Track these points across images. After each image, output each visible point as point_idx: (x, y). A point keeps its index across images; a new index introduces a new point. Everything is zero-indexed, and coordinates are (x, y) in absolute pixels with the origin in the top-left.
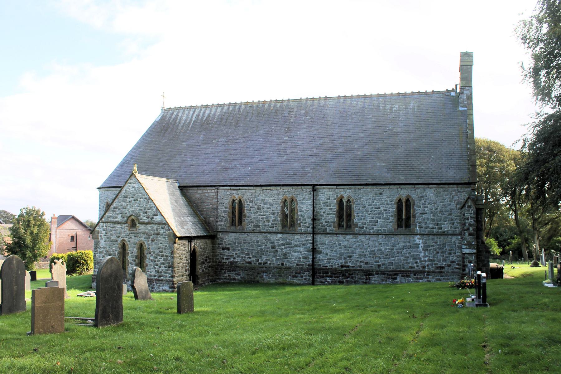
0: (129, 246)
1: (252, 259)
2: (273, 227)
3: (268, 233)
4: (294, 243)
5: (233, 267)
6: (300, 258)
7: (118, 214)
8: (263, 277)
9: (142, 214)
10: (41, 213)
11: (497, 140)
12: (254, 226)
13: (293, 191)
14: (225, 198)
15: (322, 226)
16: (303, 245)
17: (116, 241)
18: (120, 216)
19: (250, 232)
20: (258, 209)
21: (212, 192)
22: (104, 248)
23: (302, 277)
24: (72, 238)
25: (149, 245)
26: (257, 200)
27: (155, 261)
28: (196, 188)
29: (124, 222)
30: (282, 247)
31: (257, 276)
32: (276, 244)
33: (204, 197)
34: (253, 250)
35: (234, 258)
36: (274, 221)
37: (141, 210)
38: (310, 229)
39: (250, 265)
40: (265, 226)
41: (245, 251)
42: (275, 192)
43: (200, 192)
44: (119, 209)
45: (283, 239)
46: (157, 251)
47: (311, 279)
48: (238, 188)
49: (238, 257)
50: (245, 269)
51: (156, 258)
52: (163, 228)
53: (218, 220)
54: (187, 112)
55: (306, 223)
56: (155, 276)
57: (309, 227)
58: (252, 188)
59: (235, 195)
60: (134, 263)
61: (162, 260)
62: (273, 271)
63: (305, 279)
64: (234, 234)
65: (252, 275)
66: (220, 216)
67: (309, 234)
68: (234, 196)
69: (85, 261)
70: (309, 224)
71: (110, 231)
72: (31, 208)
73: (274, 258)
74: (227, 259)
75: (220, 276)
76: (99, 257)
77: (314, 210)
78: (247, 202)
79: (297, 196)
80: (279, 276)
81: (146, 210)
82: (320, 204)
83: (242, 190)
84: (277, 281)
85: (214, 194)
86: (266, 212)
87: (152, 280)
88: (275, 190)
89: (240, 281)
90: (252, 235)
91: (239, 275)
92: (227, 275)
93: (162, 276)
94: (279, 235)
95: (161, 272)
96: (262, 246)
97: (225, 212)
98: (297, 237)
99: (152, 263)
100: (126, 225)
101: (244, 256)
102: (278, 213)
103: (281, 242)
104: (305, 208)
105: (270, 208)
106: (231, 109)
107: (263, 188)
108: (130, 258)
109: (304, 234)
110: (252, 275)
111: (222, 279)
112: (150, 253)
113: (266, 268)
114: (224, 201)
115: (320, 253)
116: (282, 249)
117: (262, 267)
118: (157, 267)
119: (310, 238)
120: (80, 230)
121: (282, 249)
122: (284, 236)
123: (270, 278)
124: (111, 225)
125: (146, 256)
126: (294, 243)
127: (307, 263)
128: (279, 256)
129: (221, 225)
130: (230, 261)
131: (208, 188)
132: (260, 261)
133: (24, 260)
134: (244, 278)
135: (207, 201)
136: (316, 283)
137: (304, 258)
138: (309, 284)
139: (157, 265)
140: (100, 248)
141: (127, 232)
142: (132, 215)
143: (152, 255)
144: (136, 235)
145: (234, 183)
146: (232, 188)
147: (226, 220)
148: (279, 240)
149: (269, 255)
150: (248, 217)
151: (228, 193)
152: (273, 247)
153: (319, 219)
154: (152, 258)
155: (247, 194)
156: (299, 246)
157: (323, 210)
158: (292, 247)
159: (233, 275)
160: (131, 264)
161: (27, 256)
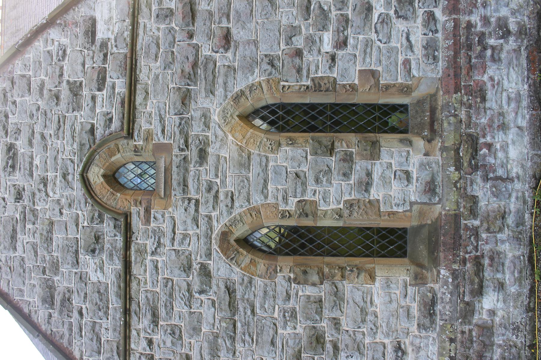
0: (257, 199)
7: (82, 278)
17: (230, 291)
25: (251, 65)
29: (120, 240)
44: (55, 267)
51: (324, 14)
56: (431, 17)
60: (360, 166)
71: (175, 333)
81: (65, 94)
87: (455, 34)
100: (137, 223)
108: (332, 200)
112: (299, 53)
124: (141, 324)
125: (317, 86)
133: (352, 153)
141: (179, 214)
143: (311, 41)
144: (193, 154)
160: (366, 185)
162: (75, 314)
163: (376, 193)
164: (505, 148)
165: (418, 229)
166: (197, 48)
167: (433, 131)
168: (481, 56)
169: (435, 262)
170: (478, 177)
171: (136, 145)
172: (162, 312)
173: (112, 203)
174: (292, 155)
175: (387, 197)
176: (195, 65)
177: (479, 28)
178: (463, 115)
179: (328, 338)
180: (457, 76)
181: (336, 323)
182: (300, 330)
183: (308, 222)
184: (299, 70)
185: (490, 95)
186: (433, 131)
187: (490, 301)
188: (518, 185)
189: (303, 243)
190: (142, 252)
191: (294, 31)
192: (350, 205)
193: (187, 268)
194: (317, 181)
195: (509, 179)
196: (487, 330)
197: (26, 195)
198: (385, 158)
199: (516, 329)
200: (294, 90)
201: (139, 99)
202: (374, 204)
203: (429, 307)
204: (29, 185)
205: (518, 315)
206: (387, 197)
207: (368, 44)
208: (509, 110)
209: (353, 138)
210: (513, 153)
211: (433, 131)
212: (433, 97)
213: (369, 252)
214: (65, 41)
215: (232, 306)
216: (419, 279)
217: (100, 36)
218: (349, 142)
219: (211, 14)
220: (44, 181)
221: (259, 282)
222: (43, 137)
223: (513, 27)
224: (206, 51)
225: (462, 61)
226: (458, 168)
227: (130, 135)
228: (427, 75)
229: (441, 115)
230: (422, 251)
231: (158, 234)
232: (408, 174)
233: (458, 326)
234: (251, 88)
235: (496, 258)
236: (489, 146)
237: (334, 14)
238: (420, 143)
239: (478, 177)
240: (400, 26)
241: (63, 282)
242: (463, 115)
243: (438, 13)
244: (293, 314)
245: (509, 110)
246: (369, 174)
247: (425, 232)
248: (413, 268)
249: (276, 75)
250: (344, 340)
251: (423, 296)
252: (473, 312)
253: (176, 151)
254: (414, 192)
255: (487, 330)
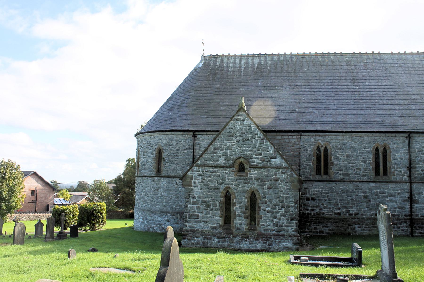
0: (236, 194)
1: (341, 209)
2: (365, 176)
3: (359, 182)
4: (388, 192)
5: (320, 219)
6: (395, 208)
7: (220, 156)
8: (354, 228)
9: (254, 156)
10: (16, 166)
11: (13, 160)
12: (343, 175)
13: (386, 138)
14: (308, 145)
15: (418, 174)
16: (399, 194)
17: (218, 189)
18: (223, 158)
19: (338, 181)
20: (348, 156)
21: (293, 138)
22: (199, 197)
23: (399, 228)
24: (33, 192)
25: (264, 193)
26: (346, 147)
27: (273, 213)
28: (275, 134)
29: (228, 165)
30: (375, 197)
31: (348, 228)
32: (368, 194)
33: (283, 144)
34: (342, 200)
35: (321, 209)
36: (365, 169)
37: (253, 151)
38: (406, 178)
39: (339, 217)
40: (355, 174)
41: (333, 201)
42: (366, 139)
43: (279, 137)
44: (222, 150)
45: (376, 189)
46: (275, 201)
47: (409, 230)
48: (325, 134)
49: (325, 208)
50: (334, 221)
51: (274, 208)
52: (283, 173)
53: (301, 168)
54: (233, 60)
55: (400, 171)
56: (273, 230)
57: (404, 176)
58: (341, 134)
59: (320, 141)
60: (243, 215)
61: (282, 211)
62: (367, 222)
63: (403, 230)
64: (320, 183)
65: (342, 227)
66: (303, 164)
67: (404, 182)
68: (319, 143)
69: (101, 213)
70: (404, 173)
71: (209, 177)
72: (6, 161)
73: (366, 209)
74: (313, 210)
75: (305, 229)
76: (193, 208)
77: (410, 159)
78: (334, 149)
79: (390, 144)
80: (373, 227)
82: (415, 152)
83: (330, 136)
84: (371, 233)
85: (296, 140)
86: (356, 159)
87: (269, 235)
88: (366, 138)
89: (328, 233)
90: (342, 184)
91: (327, 227)
92: (312, 227)
93: (284, 230)
94: (372, 184)
95: (281, 226)
96: (352, 195)
97: (309, 159)
98: (391, 186)
99: (269, 215)
101: (332, 206)
102: (369, 161)
103: (374, 191)
104: (398, 156)
105: (361, 156)
106: (282, 59)
107: (354, 134)
108: (236, 209)
109: (400, 182)
110: (342, 227)
111: (306, 232)
112: (266, 203)
113: (358, 219)
114: (307, 147)
115: (417, 202)
116: (375, 199)
117: (354, 219)
118: (275, 220)
119: (406, 187)
120: (40, 185)
121: (375, 199)
122: (378, 184)
123: (364, 230)
124: (211, 169)
125: (259, 207)
126: (388, 192)
127: (404, 213)
128: (373, 206)
129: (304, 174)
130: (315, 212)
131: (289, 134)
132: (351, 212)
134: (333, 230)
135: (288, 148)
136: (414, 234)
137: (399, 208)
138: (407, 236)
139: (275, 218)
140: (194, 197)
142: (240, 157)
143: (269, 206)
144: (246, 181)
145: (319, 129)
146: (318, 134)
147: (310, 168)
148: (371, 189)
149: (360, 206)
150: (336, 165)
151: (312, 140)
152: (365, 197)
153: (415, 168)
154: (269, 209)
155: (333, 142)
156: (395, 196)
157: (419, 159)
158: (387, 197)
159: (320, 227)
160: (239, 216)
161: (3, 208)
162: (212, 155)
163: (237, 218)
164: (246, 244)
165: (230, 226)
166: (268, 182)
167: (250, 230)
168: (265, 240)
169: (224, 229)
170: (240, 238)
171: (164, 235)
172: (214, 174)
173: (236, 164)
174: (245, 200)
175: (236, 220)
176: (264, 181)
177: (270, 240)
178: (253, 236)
179: (209, 208)
180: (261, 235)
181: (212, 210)
182: (210, 202)
183: (232, 205)
184: (262, 203)
185: (257, 241)
186: (250, 230)
187: (216, 240)
188: (238, 246)
189: (228, 200)
190: (226, 170)
191: (271, 202)
192: (235, 213)
193: (222, 180)
194: (240, 207)
195: (240, 244)
196: (210, 239)
197: (237, 143)
198: (244, 220)
199: (211, 245)
200: (259, 202)
201: (257, 169)
202: (235, 218)
203: (215, 228)
204: (239, 143)
205: (213, 245)
206: (236, 220)
207: (268, 217)
208: (254, 245)
209: (249, 214)
210: (245, 245)
211: (250, 230)
212: (257, 230)
213: (226, 216)
214: (271, 152)
215: (215, 189)
216: (220, 226)
217: (272, 160)
218: (248, 213)
219: (275, 185)
220: (240, 148)
221: (220, 194)
222: (250, 147)
223: (270, 247)
224: (267, 184)
225: (264, 236)
226: (242, 234)
227: (250, 168)
228: (261, 229)
229: (253, 232)
230: (226, 227)
231: (229, 174)
232: (241, 224)
233: (211, 234)
234: (259, 193)
235: (224, 241)
236: (246, 241)
237: (275, 211)
238: (247, 227)
239: (240, 238)
240: (272, 224)
241: (219, 152)
242: (253, 236)
243: (274, 232)
244: (213, 201)
245: (254, 245)
246: (241, 217)
247: (229, 227)
248: (223, 225)
249: (262, 198)
250: (208, 211)
251: (217, 227)
252: (214, 236)
253: (246, 177)
254: (237, 225)
255: (210, 239)
